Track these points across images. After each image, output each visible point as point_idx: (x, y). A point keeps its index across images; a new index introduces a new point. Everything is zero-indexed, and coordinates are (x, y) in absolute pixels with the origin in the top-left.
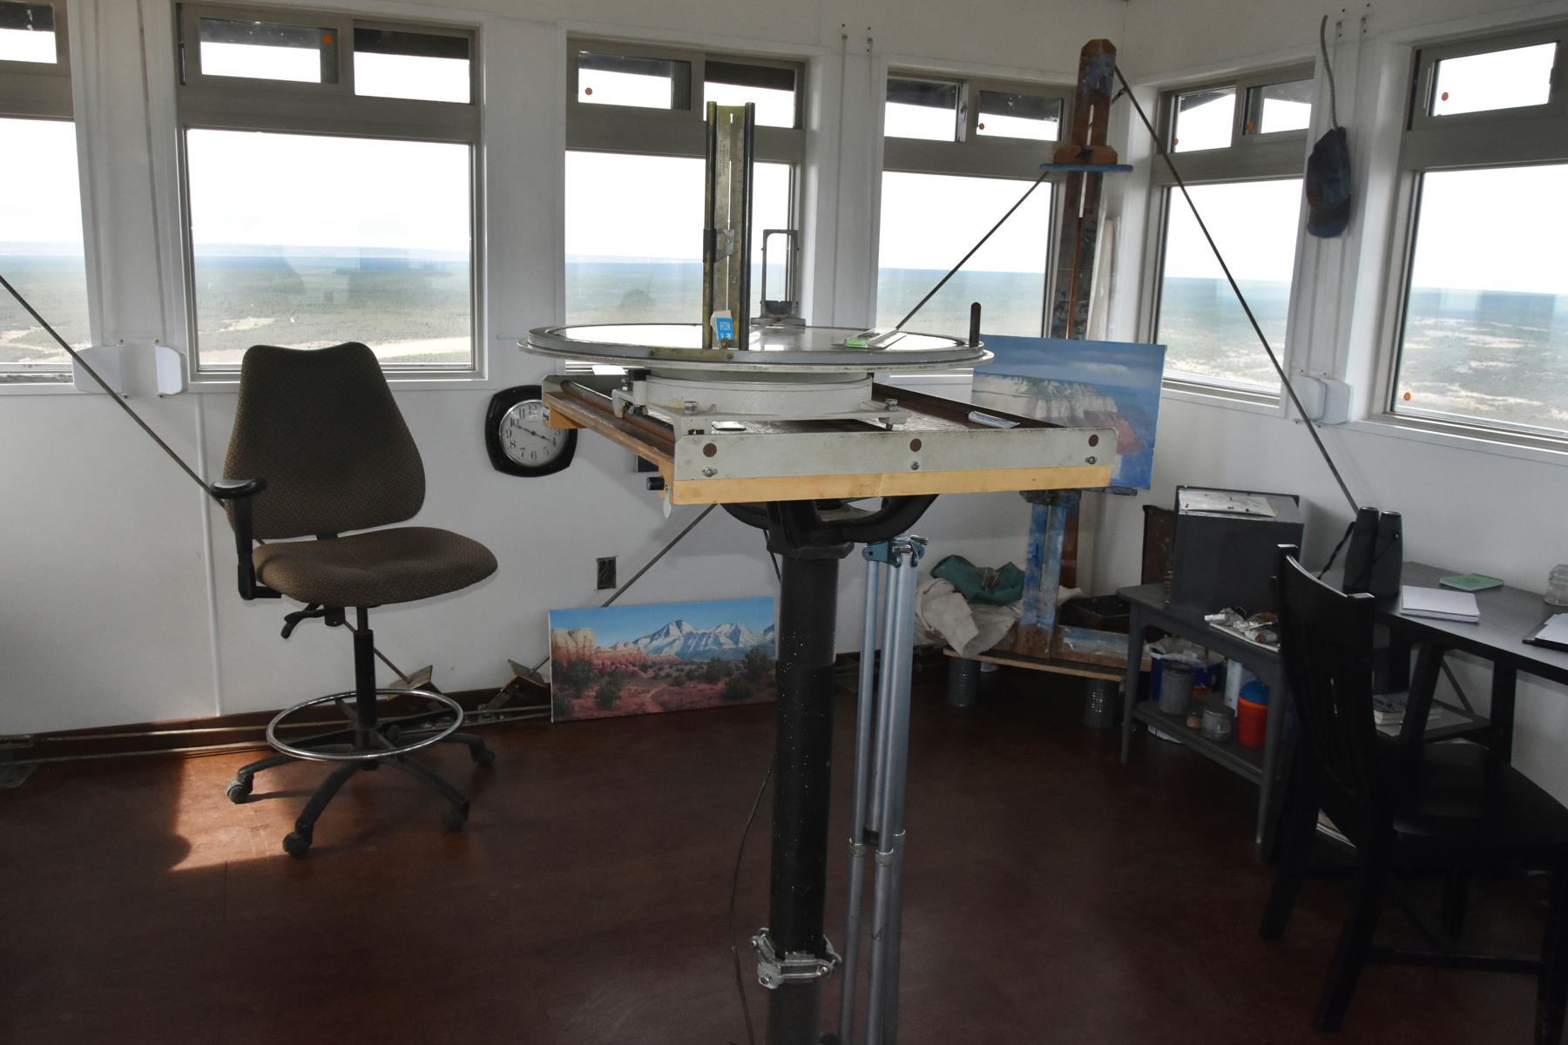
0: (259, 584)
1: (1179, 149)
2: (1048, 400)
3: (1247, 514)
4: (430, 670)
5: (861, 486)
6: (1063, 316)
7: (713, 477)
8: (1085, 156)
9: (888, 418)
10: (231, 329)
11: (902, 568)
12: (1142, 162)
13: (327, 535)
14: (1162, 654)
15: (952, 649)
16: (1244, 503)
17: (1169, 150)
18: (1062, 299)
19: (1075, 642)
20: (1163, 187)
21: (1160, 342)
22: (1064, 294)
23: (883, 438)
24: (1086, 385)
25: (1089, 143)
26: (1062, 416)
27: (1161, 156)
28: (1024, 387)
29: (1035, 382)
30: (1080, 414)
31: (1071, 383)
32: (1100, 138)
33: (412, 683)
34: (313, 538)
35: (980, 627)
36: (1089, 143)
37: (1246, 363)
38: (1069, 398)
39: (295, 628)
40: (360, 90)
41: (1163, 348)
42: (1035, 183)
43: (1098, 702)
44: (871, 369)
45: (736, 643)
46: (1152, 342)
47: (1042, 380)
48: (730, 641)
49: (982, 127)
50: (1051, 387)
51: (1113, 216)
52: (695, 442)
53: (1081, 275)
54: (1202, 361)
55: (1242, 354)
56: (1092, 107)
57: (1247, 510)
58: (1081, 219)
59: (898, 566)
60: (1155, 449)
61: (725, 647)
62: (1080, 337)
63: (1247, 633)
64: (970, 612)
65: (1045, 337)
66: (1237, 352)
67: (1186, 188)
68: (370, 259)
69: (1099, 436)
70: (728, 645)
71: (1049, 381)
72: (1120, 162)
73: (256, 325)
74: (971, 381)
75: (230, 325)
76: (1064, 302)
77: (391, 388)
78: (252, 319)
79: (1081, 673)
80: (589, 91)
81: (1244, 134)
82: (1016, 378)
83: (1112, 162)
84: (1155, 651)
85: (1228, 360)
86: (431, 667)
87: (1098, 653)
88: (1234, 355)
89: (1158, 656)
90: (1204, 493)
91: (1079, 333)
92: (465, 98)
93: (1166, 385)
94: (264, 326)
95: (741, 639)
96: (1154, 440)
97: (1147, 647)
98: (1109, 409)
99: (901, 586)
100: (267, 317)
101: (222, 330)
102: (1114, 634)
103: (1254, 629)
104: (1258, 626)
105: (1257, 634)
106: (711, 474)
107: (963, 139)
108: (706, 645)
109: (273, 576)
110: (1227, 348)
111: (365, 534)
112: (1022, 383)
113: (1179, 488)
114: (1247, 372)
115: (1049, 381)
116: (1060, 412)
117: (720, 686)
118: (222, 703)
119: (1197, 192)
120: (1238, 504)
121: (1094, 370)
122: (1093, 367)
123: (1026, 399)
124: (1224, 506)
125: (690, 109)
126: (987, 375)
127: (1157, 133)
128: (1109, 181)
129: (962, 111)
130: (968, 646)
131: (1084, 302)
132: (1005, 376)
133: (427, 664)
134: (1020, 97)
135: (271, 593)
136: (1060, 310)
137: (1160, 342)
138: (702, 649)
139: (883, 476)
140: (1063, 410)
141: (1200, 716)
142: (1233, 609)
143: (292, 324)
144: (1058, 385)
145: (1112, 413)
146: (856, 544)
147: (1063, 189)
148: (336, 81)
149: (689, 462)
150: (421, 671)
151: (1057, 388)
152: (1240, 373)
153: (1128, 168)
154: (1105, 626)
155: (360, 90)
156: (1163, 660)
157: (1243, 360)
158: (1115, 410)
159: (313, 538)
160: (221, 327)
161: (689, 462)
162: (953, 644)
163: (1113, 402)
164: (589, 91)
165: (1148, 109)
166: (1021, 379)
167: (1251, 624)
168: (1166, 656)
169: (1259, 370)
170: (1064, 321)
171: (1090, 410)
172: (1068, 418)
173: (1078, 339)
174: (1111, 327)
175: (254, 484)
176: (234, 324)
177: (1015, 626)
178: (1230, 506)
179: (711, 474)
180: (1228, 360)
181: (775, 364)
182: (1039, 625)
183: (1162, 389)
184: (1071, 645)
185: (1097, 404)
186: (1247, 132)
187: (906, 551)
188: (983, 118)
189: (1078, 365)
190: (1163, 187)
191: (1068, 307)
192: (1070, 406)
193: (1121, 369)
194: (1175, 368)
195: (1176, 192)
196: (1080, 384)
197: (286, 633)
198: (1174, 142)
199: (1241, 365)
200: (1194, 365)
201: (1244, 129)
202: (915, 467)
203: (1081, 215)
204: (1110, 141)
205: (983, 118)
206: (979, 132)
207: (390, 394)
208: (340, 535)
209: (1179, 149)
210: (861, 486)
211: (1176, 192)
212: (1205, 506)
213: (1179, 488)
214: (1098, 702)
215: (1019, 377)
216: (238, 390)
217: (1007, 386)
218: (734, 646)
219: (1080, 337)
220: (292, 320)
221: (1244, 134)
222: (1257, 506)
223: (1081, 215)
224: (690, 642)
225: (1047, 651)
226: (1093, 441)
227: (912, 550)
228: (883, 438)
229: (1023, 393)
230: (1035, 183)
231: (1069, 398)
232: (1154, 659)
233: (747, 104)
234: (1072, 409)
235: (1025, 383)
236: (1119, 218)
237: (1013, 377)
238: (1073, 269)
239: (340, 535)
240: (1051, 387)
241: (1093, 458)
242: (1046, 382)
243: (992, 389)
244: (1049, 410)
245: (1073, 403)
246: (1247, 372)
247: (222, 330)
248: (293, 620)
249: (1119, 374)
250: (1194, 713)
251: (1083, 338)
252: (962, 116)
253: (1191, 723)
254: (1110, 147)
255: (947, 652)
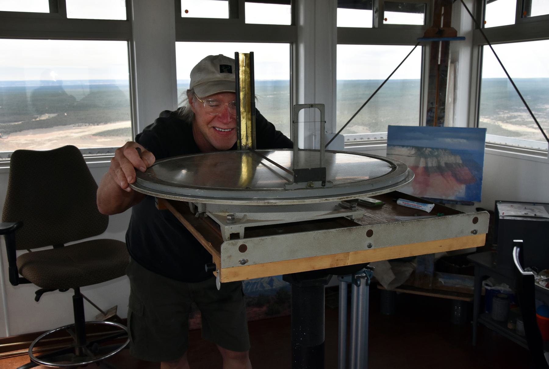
0: (20, 276)
1: (487, 26)
2: (426, 157)
3: (535, 217)
4: (116, 308)
5: (337, 260)
6: (432, 115)
7: (245, 265)
8: (440, 33)
9: (352, 215)
10: (38, 119)
11: (361, 287)
12: (468, 33)
13: (58, 245)
14: (491, 286)
15: (381, 285)
16: (533, 210)
17: (481, 27)
18: (431, 106)
19: (444, 281)
20: (479, 46)
21: (480, 126)
22: (432, 103)
23: (350, 231)
24: (445, 150)
25: (442, 26)
26: (434, 166)
27: (478, 30)
28: (413, 152)
29: (419, 149)
30: (443, 164)
31: (437, 149)
32: (448, 23)
33: (107, 315)
34: (51, 247)
35: (395, 274)
36: (442, 26)
37: (507, 117)
38: (437, 157)
39: (41, 297)
40: (69, 16)
41: (484, 131)
42: (414, 46)
43: (458, 311)
44: (342, 199)
45: (272, 286)
46: (476, 127)
47: (422, 148)
48: (269, 286)
49: (386, 20)
50: (427, 151)
51: (455, 61)
52: (234, 245)
53: (440, 94)
54: (487, 117)
55: (506, 113)
56: (443, 8)
57: (535, 215)
58: (439, 65)
59: (358, 286)
60: (482, 181)
61: (267, 288)
62: (441, 125)
63: (540, 282)
64: (390, 266)
65: (421, 125)
66: (503, 112)
67: (492, 46)
68: (100, 85)
69: (478, 217)
70: (268, 287)
71: (426, 148)
72: (458, 36)
73: (49, 117)
74: (386, 148)
75: (37, 117)
76: (432, 108)
77: (89, 166)
78: (47, 114)
79: (449, 297)
80: (187, 11)
81: (522, 17)
82: (409, 147)
83: (454, 35)
84: (487, 285)
85: (499, 116)
86: (117, 306)
87: (457, 286)
88: (502, 113)
89: (489, 288)
90: (510, 205)
91: (441, 123)
92: (124, 18)
93: (488, 146)
94: (53, 117)
95: (274, 284)
96: (482, 177)
97: (484, 282)
98: (458, 161)
99: (361, 297)
100: (54, 113)
101: (34, 120)
102: (465, 276)
103: (544, 280)
104: (546, 278)
105: (546, 283)
106: (244, 262)
107: (377, 26)
108: (257, 288)
109: (27, 273)
110: (498, 110)
111: (81, 239)
112: (412, 149)
113: (497, 202)
114: (508, 121)
115: (426, 148)
116: (432, 164)
117: (264, 309)
118: (9, 330)
119: (499, 48)
120: (530, 211)
121: (449, 141)
122: (448, 140)
123: (414, 158)
124: (522, 213)
125: (238, 18)
126: (394, 146)
127: (475, 18)
128: (453, 45)
129: (376, 12)
130: (391, 283)
131: (442, 107)
132: (403, 146)
133: (115, 305)
134: (404, 4)
135: (25, 281)
136: (430, 112)
137: (480, 126)
138: (254, 290)
139: (350, 253)
140: (434, 162)
141: (515, 323)
142: (531, 268)
143: (66, 116)
144: (431, 150)
145: (459, 163)
146: (333, 275)
147: (428, 49)
148: (57, 12)
149: (230, 257)
150: (111, 308)
151: (430, 152)
152: (505, 122)
153: (463, 38)
154: (461, 272)
155: (69, 16)
156: (491, 290)
157: (506, 115)
158: (461, 162)
159: (51, 247)
160: (33, 119)
161: (230, 257)
162: (382, 283)
163: (460, 158)
164: (187, 11)
165: (470, 6)
166: (411, 148)
167: (542, 277)
168: (493, 288)
169: (514, 120)
170: (433, 117)
171: (448, 162)
172: (436, 166)
173: (440, 126)
174: (456, 117)
175: (15, 226)
176: (39, 117)
177: (413, 273)
178: (526, 213)
179: (244, 262)
180: (499, 116)
181: (278, 220)
182: (426, 272)
183: (486, 149)
184: (443, 282)
185: (452, 159)
186: (523, 16)
187: (363, 277)
188: (387, 14)
189: (440, 139)
190: (479, 46)
191: (434, 110)
192: (438, 160)
193: (464, 141)
194: (489, 138)
195: (486, 48)
196: (442, 149)
197: (37, 299)
198: (484, 22)
199: (505, 118)
200: (483, 119)
201: (522, 15)
202: (370, 246)
203: (439, 63)
204: (453, 25)
205: (387, 14)
206: (385, 22)
207: (88, 169)
208: (66, 245)
209: (487, 26)
210: (337, 260)
211: (486, 48)
212: (513, 213)
213: (497, 202)
214: (458, 311)
215: (410, 146)
216: (9, 171)
217: (404, 151)
218: (270, 288)
219: (441, 125)
220: (66, 114)
221: (522, 17)
222: (540, 212)
223: (439, 63)
224: (248, 287)
225: (430, 285)
226: (475, 221)
227: (366, 276)
228: (350, 231)
229: (413, 155)
230: (414, 46)
231: (437, 157)
232: (487, 290)
233: (250, 52)
234: (439, 162)
235: (414, 149)
236: (457, 62)
237: (407, 146)
238: (436, 91)
239: (66, 245)
240: (427, 151)
241: (475, 230)
242: (424, 149)
243: (397, 153)
244: (426, 163)
245: (439, 159)
246: (508, 121)
247: (34, 120)
248: (39, 295)
249: (462, 143)
250: (511, 321)
251: (443, 126)
252: (376, 15)
253: (510, 326)
254: (453, 28)
255: (379, 287)
